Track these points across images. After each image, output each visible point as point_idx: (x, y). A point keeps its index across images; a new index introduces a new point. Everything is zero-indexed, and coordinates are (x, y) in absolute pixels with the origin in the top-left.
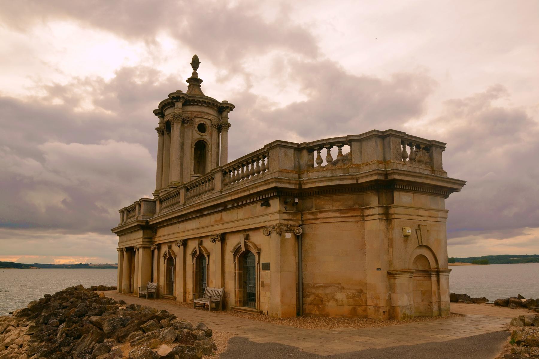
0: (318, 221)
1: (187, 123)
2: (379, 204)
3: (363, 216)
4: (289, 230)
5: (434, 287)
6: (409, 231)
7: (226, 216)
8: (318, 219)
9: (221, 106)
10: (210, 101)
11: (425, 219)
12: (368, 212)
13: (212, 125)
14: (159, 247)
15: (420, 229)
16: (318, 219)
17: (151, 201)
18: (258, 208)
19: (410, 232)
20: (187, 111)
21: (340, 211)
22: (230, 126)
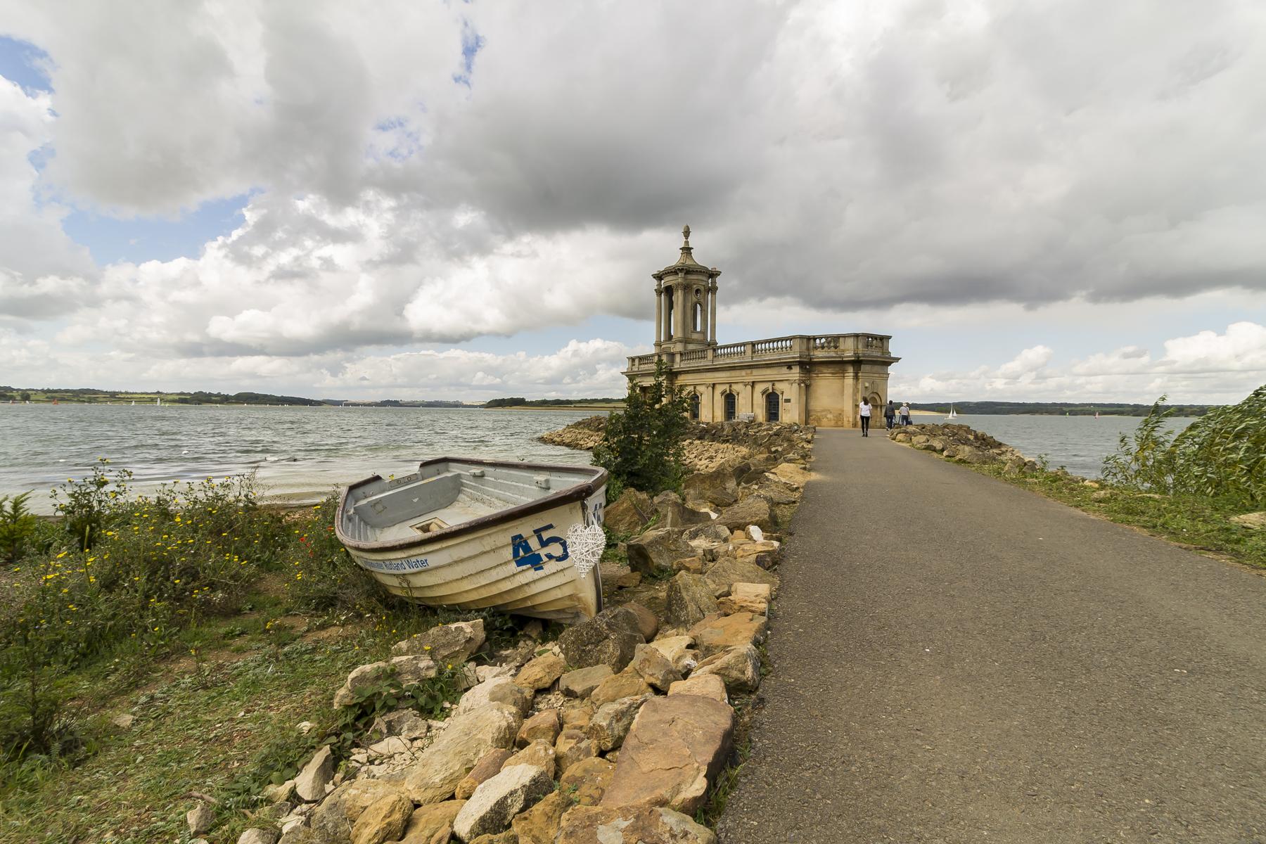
4: (803, 382)
6: (867, 385)
7: (755, 372)
12: (846, 375)
18: (785, 370)
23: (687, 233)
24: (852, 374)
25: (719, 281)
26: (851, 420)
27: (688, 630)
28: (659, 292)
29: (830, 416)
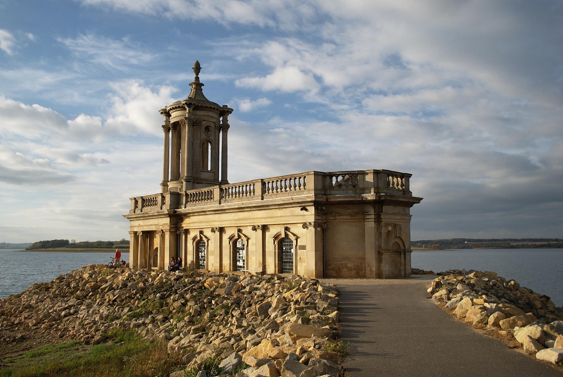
0: (337, 221)
1: (196, 126)
2: (374, 212)
3: (364, 219)
5: (403, 261)
8: (337, 219)
9: (223, 111)
10: (215, 107)
11: (399, 221)
12: (368, 217)
13: (216, 127)
14: (187, 232)
15: (396, 227)
16: (337, 219)
17: (175, 194)
18: (298, 210)
19: (391, 229)
20: (196, 115)
21: (351, 215)
22: (229, 127)
23: (197, 69)
24: (373, 217)
25: (231, 118)
26: (374, 269)
27: (332, 348)
28: (167, 128)
29: (349, 265)
